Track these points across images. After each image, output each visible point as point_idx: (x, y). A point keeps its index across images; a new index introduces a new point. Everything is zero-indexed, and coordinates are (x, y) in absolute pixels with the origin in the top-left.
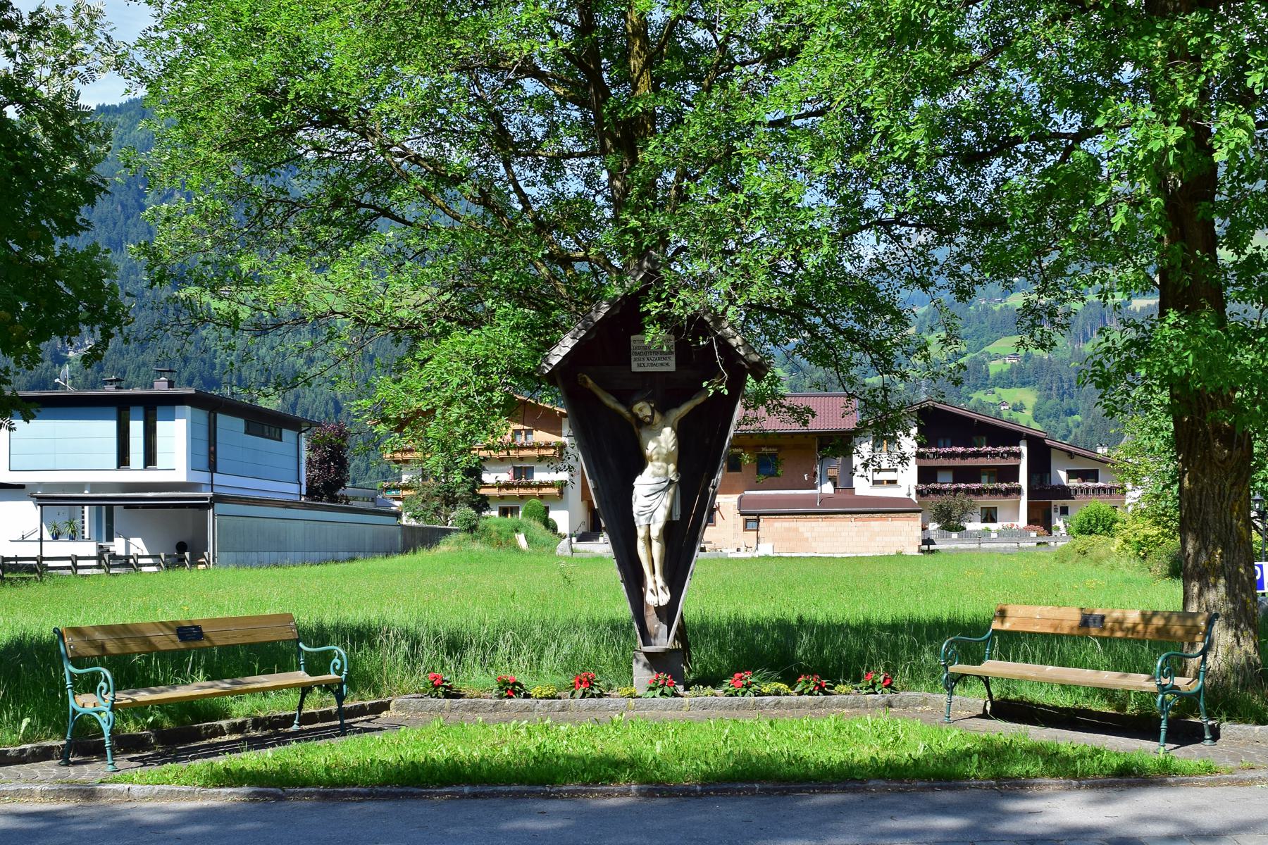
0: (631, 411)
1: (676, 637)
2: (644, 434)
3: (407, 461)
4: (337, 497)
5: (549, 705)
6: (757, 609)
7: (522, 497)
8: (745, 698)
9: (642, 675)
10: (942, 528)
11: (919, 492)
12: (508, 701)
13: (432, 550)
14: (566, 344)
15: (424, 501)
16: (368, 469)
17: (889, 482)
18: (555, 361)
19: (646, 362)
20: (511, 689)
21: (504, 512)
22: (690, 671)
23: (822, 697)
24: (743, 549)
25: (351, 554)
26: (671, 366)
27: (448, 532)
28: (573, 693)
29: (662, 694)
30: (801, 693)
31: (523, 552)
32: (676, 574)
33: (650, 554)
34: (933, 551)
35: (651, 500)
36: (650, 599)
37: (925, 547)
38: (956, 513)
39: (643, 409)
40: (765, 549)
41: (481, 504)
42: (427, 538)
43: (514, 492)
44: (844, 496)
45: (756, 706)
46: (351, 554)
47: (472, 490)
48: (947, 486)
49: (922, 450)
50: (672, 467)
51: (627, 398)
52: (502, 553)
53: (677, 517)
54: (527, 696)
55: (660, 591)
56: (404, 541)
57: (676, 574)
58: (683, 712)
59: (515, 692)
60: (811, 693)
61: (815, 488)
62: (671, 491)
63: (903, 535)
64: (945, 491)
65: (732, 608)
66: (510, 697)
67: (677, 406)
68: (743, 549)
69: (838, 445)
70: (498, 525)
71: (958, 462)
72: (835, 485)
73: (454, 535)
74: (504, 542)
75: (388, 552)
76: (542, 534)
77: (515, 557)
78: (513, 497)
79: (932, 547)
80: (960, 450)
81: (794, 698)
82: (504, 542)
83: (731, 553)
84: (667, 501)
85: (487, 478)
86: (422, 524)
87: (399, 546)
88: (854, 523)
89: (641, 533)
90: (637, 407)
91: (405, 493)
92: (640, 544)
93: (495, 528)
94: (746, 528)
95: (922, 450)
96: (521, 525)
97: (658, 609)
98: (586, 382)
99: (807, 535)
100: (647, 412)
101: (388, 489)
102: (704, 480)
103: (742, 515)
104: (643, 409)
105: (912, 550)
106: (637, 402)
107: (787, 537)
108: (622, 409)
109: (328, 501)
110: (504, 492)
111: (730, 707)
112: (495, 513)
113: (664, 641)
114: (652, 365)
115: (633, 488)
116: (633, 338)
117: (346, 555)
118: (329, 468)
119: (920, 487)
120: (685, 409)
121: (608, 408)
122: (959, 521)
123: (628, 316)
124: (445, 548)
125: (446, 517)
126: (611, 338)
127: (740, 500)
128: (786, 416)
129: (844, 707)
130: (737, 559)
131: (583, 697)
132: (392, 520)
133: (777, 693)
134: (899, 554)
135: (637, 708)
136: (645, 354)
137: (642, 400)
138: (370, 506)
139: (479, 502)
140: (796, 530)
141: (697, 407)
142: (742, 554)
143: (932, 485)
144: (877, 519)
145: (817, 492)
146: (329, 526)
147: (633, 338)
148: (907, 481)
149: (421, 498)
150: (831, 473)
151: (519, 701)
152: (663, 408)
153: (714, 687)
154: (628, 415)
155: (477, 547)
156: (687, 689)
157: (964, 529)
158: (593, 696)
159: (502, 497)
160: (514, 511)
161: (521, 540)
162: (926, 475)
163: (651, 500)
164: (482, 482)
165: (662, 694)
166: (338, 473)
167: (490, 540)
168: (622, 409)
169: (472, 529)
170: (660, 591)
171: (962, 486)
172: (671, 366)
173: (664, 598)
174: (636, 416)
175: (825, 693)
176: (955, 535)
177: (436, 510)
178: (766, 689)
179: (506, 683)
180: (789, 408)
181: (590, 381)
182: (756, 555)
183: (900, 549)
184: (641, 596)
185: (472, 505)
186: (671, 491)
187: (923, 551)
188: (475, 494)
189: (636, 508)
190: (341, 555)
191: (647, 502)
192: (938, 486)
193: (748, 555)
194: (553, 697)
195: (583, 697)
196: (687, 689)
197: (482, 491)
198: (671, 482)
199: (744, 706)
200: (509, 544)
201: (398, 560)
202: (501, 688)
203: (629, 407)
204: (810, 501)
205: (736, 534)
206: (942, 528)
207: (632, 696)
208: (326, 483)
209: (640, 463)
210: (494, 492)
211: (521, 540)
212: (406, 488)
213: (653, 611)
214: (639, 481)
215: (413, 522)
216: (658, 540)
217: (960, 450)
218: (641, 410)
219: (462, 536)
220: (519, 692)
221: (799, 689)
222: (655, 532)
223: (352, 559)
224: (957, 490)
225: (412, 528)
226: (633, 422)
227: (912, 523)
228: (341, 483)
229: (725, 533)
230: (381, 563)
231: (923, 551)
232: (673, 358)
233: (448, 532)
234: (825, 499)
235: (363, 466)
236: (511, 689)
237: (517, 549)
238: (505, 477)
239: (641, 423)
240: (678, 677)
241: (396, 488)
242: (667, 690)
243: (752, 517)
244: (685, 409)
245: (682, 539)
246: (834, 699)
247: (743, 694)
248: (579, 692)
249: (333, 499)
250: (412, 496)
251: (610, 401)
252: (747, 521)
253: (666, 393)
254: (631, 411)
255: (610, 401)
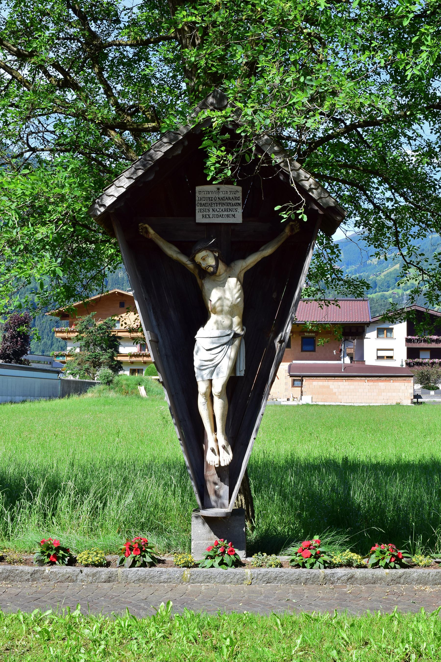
0: (193, 260)
1: (240, 492)
2: (207, 285)
3: (70, 339)
4: (21, 360)
5: (94, 575)
6: (310, 448)
7: (145, 363)
8: (315, 571)
9: (201, 536)
10: (424, 388)
11: (407, 364)
12: (47, 569)
13: (81, 396)
14: (124, 183)
15: (79, 364)
16: (52, 345)
17: (388, 357)
18: (108, 201)
19: (211, 213)
20: (57, 554)
21: (133, 372)
22: (253, 529)
23: (401, 571)
24: (291, 399)
25: (24, 398)
26: (237, 217)
27: (94, 384)
28: (122, 560)
29: (221, 563)
30: (376, 565)
31: (142, 398)
32: (239, 430)
33: (212, 411)
34: (421, 403)
35: (214, 354)
36: (211, 459)
37: (415, 400)
38: (433, 378)
39: (207, 259)
40: (307, 399)
41: (117, 367)
42: (80, 388)
43: (140, 359)
44: (356, 364)
45: (326, 580)
46: (24, 398)
47: (112, 358)
48: (427, 360)
49: (409, 337)
50: (236, 320)
51: (188, 249)
52: (127, 399)
53: (241, 372)
54: (72, 562)
55: (221, 450)
56: (63, 390)
57: (239, 430)
58: (244, 586)
59: (58, 558)
60: (387, 566)
61: (341, 360)
62: (237, 342)
63: (403, 391)
64: (425, 364)
65: (288, 447)
66: (52, 563)
67: (244, 257)
68: (291, 399)
69: (354, 332)
70: (127, 380)
71: (433, 345)
72: (351, 359)
73: (97, 386)
74: (130, 391)
75: (51, 396)
76: (157, 387)
77: (137, 401)
78: (139, 363)
79: (420, 400)
80: (435, 337)
81: (370, 572)
82: (130, 391)
83: (284, 402)
84: (232, 352)
85: (122, 350)
86: (77, 378)
87: (59, 393)
88: (367, 384)
89: (202, 387)
90: (199, 257)
91: (69, 359)
92: (201, 400)
93: (125, 382)
94: (293, 385)
95: (409, 337)
96: (142, 380)
97: (220, 470)
98: (147, 232)
99: (335, 390)
100: (211, 262)
101: (57, 356)
102: (272, 335)
103: (291, 376)
104: (207, 259)
105: (407, 402)
106: (199, 251)
107: (316, 392)
108: (184, 259)
109: (16, 363)
110: (134, 359)
111: (297, 581)
112: (127, 373)
113: (225, 502)
114: (218, 216)
115: (195, 341)
116: (198, 188)
117: (9, 398)
118: (17, 341)
119: (409, 361)
120: (252, 260)
121: (169, 259)
122: (435, 383)
123: (189, 154)
124: (89, 395)
125: (94, 374)
126: (172, 182)
127: (290, 366)
128: (344, 289)
129: (425, 584)
130: (287, 406)
131: (133, 565)
132: (54, 376)
133: (349, 564)
134: (398, 404)
135: (191, 580)
136: (211, 205)
137: (205, 249)
138: (47, 367)
139: (116, 365)
140: (328, 387)
141: (264, 259)
142: (291, 403)
143: (416, 360)
144: (383, 381)
145: (342, 362)
146: (10, 379)
147: (198, 188)
148: (400, 358)
149: (77, 362)
150: (348, 351)
151: (61, 569)
152: (228, 258)
153: (276, 555)
154: (190, 265)
155: (112, 394)
156: (249, 555)
157: (438, 388)
158: (144, 565)
159: (132, 363)
160: (140, 371)
161: (142, 390)
162: (412, 353)
163: (214, 354)
164: (118, 352)
165: (221, 563)
166: (23, 345)
167: (121, 391)
168: (184, 259)
169: (109, 382)
170: (221, 450)
171: (436, 360)
172: (237, 217)
173: (226, 458)
174: (198, 266)
175: (403, 566)
176: (432, 393)
177: (87, 370)
178: (337, 559)
179: (49, 548)
180: (345, 282)
181: (151, 231)
182: (300, 403)
183: (399, 401)
184: (202, 454)
185: (111, 367)
186: (237, 342)
187: (414, 403)
188: (113, 360)
189: (196, 364)
190: (17, 398)
191: (208, 356)
192: (420, 360)
193: (295, 403)
194: (100, 565)
195: (133, 565)
196: (249, 555)
197: (119, 359)
198: (236, 335)
199: (314, 580)
200: (132, 393)
201: (58, 402)
202: (43, 553)
203: (191, 256)
204: (338, 368)
205: (286, 390)
206: (424, 388)
207: (187, 566)
208: (14, 351)
209: (202, 316)
210: (127, 359)
211: (142, 390)
212: (69, 356)
213: (213, 471)
214: (201, 333)
215: (71, 378)
216: (220, 397)
217: (435, 337)
218: (204, 259)
219: (102, 387)
220: (63, 558)
221: (373, 559)
222: (218, 386)
223: (24, 401)
224: (433, 363)
225: (69, 381)
226: (196, 273)
227: (406, 384)
228: (24, 352)
229: (281, 388)
230: (44, 404)
231: (414, 403)
232: (240, 210)
233: (94, 384)
234: (346, 367)
235: (49, 343)
236: (57, 554)
237: (138, 396)
238: (135, 349)
239: (204, 273)
240: (238, 541)
241: (62, 356)
242: (227, 559)
243: (298, 378)
244: (252, 260)
245: (245, 396)
246: (414, 572)
247: (312, 565)
248: (129, 560)
249: (19, 361)
250: (71, 361)
251: (172, 252)
252: (294, 380)
253: (231, 245)
254: (193, 260)
255: (172, 252)
